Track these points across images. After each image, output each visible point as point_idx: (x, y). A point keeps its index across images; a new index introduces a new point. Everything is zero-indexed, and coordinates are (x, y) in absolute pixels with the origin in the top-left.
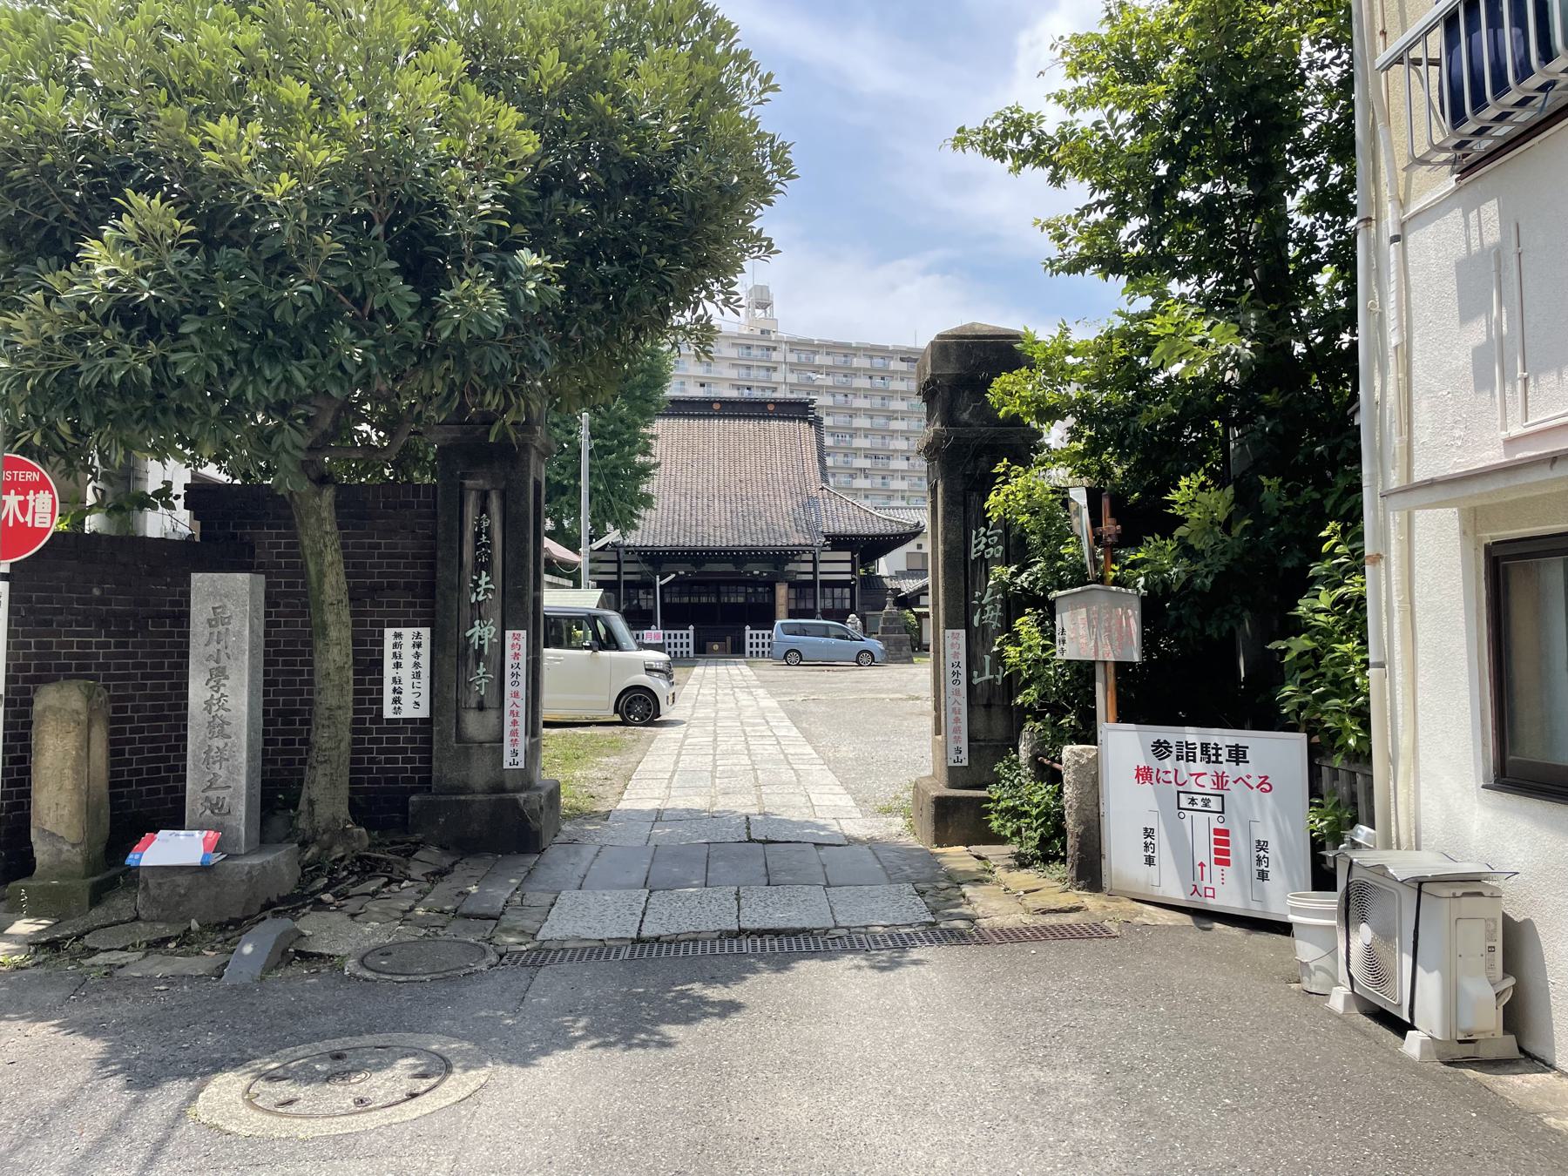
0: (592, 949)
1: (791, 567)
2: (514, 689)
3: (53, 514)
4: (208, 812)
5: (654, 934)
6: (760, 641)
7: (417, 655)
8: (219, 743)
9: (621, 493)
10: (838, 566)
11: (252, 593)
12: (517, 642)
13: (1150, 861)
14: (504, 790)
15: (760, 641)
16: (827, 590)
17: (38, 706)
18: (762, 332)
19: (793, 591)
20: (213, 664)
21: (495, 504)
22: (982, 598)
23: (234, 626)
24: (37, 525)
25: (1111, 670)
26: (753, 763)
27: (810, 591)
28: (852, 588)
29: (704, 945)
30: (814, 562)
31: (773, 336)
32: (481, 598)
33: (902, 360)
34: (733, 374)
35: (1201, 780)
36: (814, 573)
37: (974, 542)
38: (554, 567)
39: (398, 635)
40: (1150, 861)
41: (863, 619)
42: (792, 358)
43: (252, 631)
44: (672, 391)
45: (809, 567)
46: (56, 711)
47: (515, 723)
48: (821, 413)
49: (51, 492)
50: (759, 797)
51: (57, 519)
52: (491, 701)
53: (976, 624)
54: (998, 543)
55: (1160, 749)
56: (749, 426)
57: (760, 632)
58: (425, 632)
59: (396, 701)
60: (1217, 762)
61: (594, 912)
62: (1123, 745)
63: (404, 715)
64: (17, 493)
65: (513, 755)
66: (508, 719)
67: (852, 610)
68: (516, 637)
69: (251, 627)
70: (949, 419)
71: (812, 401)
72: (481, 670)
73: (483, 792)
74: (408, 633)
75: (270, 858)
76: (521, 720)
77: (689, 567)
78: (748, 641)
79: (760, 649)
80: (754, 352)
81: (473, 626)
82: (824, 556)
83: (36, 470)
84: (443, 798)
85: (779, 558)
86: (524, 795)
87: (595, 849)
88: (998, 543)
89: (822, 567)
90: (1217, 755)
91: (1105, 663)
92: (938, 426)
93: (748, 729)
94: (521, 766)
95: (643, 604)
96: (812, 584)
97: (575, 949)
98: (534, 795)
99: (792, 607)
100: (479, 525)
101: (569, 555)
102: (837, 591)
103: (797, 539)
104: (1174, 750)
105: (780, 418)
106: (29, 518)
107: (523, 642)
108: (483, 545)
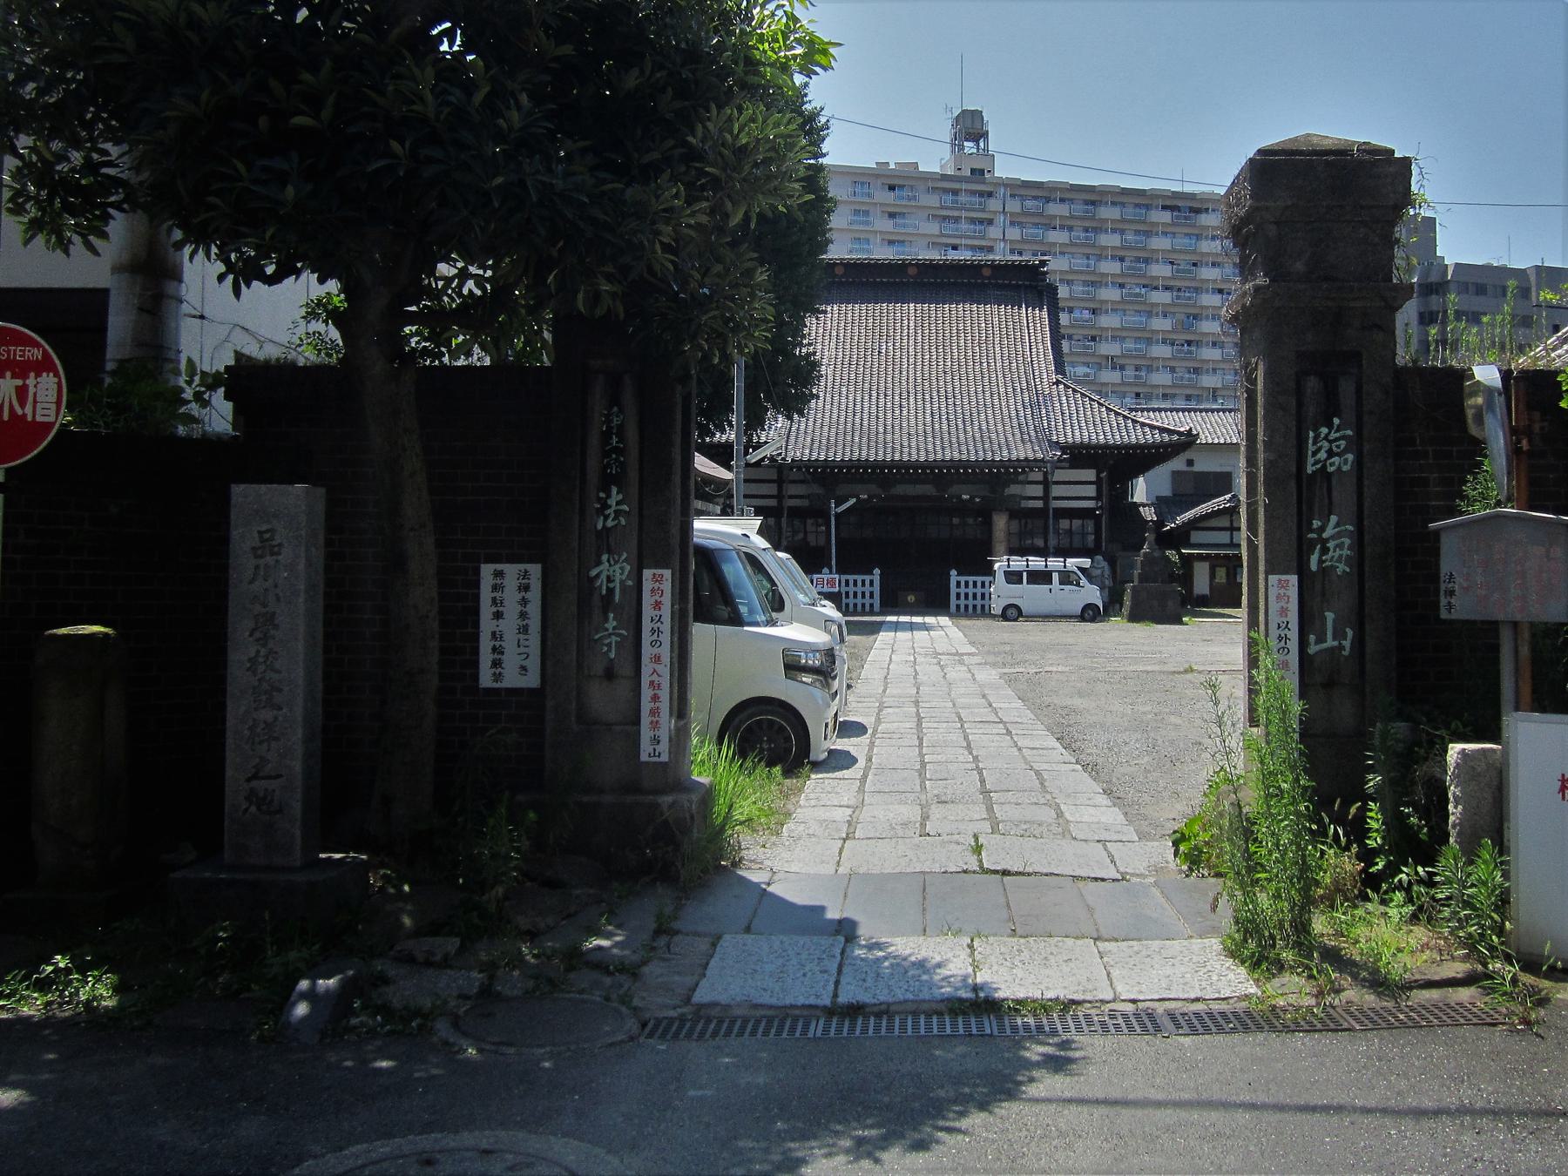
0: (770, 1021)
1: (1014, 489)
2: (656, 651)
3: (58, 403)
4: (253, 809)
7: (524, 602)
8: (267, 715)
9: (787, 382)
12: (659, 586)
18: (973, 171)
19: (1015, 525)
20: (258, 608)
22: (1322, 529)
23: (286, 555)
24: (39, 419)
25: (1526, 635)
26: (976, 758)
28: (1097, 519)
32: (610, 523)
33: (1164, 208)
34: (933, 228)
36: (1046, 497)
37: (1311, 448)
39: (499, 574)
44: (838, 251)
47: (655, 698)
49: (56, 375)
50: (990, 809)
51: (63, 409)
52: (626, 670)
53: (1314, 566)
54: (1346, 451)
57: (971, 579)
58: (535, 570)
59: (496, 664)
63: (507, 683)
65: (653, 744)
66: (646, 693)
68: (657, 579)
70: (1277, 273)
71: (1043, 263)
74: (512, 570)
76: (665, 694)
77: (873, 488)
79: (971, 602)
80: (963, 198)
81: (599, 563)
82: (1060, 475)
83: (38, 345)
86: (669, 799)
88: (1346, 451)
91: (1515, 625)
92: (1261, 280)
93: (963, 714)
94: (665, 758)
95: (812, 539)
96: (1042, 513)
98: (683, 798)
100: (608, 421)
103: (1021, 452)
106: (29, 409)
107: (667, 586)
108: (616, 450)
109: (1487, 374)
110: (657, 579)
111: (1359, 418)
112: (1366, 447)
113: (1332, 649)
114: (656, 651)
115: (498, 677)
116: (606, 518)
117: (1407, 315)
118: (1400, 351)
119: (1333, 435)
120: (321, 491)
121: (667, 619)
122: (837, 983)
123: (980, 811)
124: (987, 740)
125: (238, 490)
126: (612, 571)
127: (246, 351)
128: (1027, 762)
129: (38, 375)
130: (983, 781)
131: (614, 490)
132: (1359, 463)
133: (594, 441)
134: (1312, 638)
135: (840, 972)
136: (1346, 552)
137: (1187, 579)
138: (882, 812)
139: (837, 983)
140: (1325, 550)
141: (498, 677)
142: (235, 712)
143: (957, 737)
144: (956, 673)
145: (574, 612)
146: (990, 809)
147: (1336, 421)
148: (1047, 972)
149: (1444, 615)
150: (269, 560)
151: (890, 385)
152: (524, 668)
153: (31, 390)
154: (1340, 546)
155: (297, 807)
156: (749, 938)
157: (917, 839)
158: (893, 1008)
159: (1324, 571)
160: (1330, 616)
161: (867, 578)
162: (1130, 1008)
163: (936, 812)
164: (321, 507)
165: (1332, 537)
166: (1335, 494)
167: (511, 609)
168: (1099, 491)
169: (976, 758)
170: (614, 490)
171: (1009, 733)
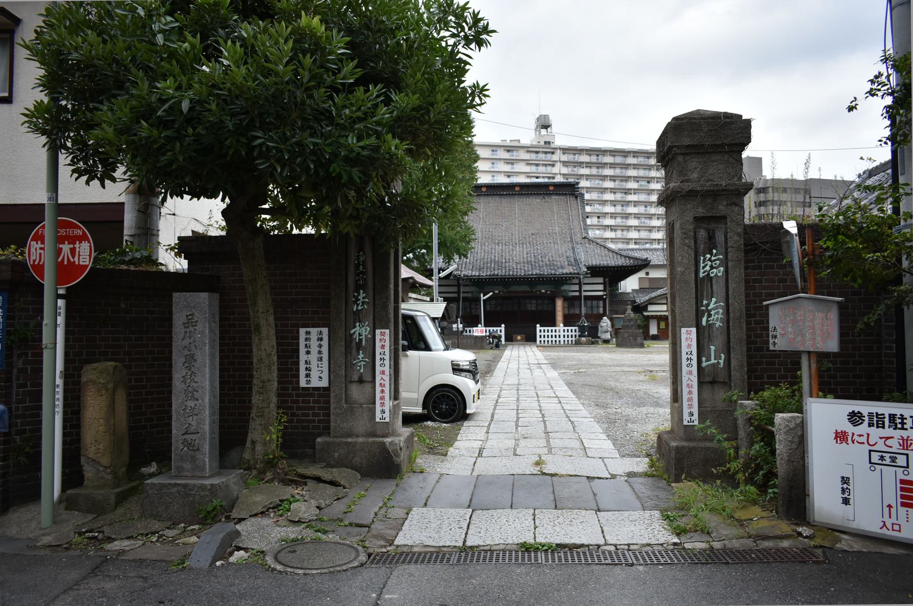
0: (432, 553)
1: (565, 287)
2: (382, 369)
4: (185, 449)
5: (475, 544)
6: (546, 334)
7: (320, 346)
8: (191, 403)
10: (596, 288)
11: (210, 305)
12: (384, 339)
13: (846, 501)
14: (376, 436)
15: (546, 334)
16: (589, 302)
17: (84, 379)
18: (545, 143)
20: (187, 352)
21: (368, 247)
22: (708, 305)
23: (199, 327)
24: (81, 263)
26: (543, 415)
27: (577, 303)
29: (510, 555)
30: (580, 284)
31: (552, 146)
32: (360, 308)
35: (889, 442)
36: (580, 291)
37: (702, 265)
38: (412, 286)
39: (308, 333)
40: (846, 501)
41: (611, 319)
42: (565, 158)
43: (211, 331)
45: (576, 288)
46: (94, 382)
47: (383, 391)
48: (584, 191)
49: (89, 242)
50: (548, 441)
53: (704, 323)
54: (719, 266)
55: (855, 418)
56: (536, 201)
58: (325, 331)
59: (308, 376)
60: (903, 428)
61: (434, 525)
62: (825, 415)
64: (69, 243)
66: (378, 389)
67: (604, 314)
68: (383, 334)
69: (210, 328)
72: (361, 356)
73: (363, 436)
74: (314, 331)
75: (224, 480)
78: (538, 334)
81: (355, 327)
83: (80, 228)
84: (337, 440)
85: (557, 282)
86: (389, 440)
87: (436, 477)
88: (719, 266)
89: (585, 287)
90: (903, 423)
91: (809, 353)
94: (387, 420)
97: (420, 554)
99: (566, 312)
100: (358, 259)
101: (427, 282)
102: (595, 302)
103: (568, 270)
104: (866, 419)
105: (557, 194)
106: (76, 259)
107: (387, 338)
108: (362, 272)
109: (791, 226)
110: (383, 334)
111: (726, 249)
112: (730, 264)
113: (713, 365)
114: (382, 369)
115: (308, 382)
116: (358, 305)
117: (749, 200)
118: (747, 216)
119: (713, 258)
120: (216, 296)
121: (387, 353)
122: (466, 534)
123: (543, 443)
124: (550, 406)
125: (176, 295)
126: (361, 331)
127: (196, 230)
128: (567, 417)
129: (80, 242)
130: (545, 427)
131: (361, 291)
132: (726, 272)
133: (352, 268)
134: (704, 359)
135: (468, 528)
136: (720, 316)
137: (646, 328)
138: (499, 442)
139: (466, 534)
140: (709, 316)
141: (308, 382)
142: (176, 403)
143: (535, 405)
144: (537, 372)
145: (347, 353)
146: (548, 441)
147: (714, 251)
148: (571, 528)
149: (771, 348)
150: (191, 329)
151: (501, 242)
152: (320, 377)
153: (77, 250)
154: (717, 313)
155: (207, 448)
156: (425, 510)
157: (512, 457)
158: (493, 548)
159: (710, 326)
160: (713, 348)
161: (499, 329)
162: (612, 548)
163: (523, 443)
164: (216, 303)
165: (713, 309)
166: (714, 287)
167: (314, 349)
168: (605, 287)
169: (543, 415)
170: (361, 291)
171: (560, 402)
